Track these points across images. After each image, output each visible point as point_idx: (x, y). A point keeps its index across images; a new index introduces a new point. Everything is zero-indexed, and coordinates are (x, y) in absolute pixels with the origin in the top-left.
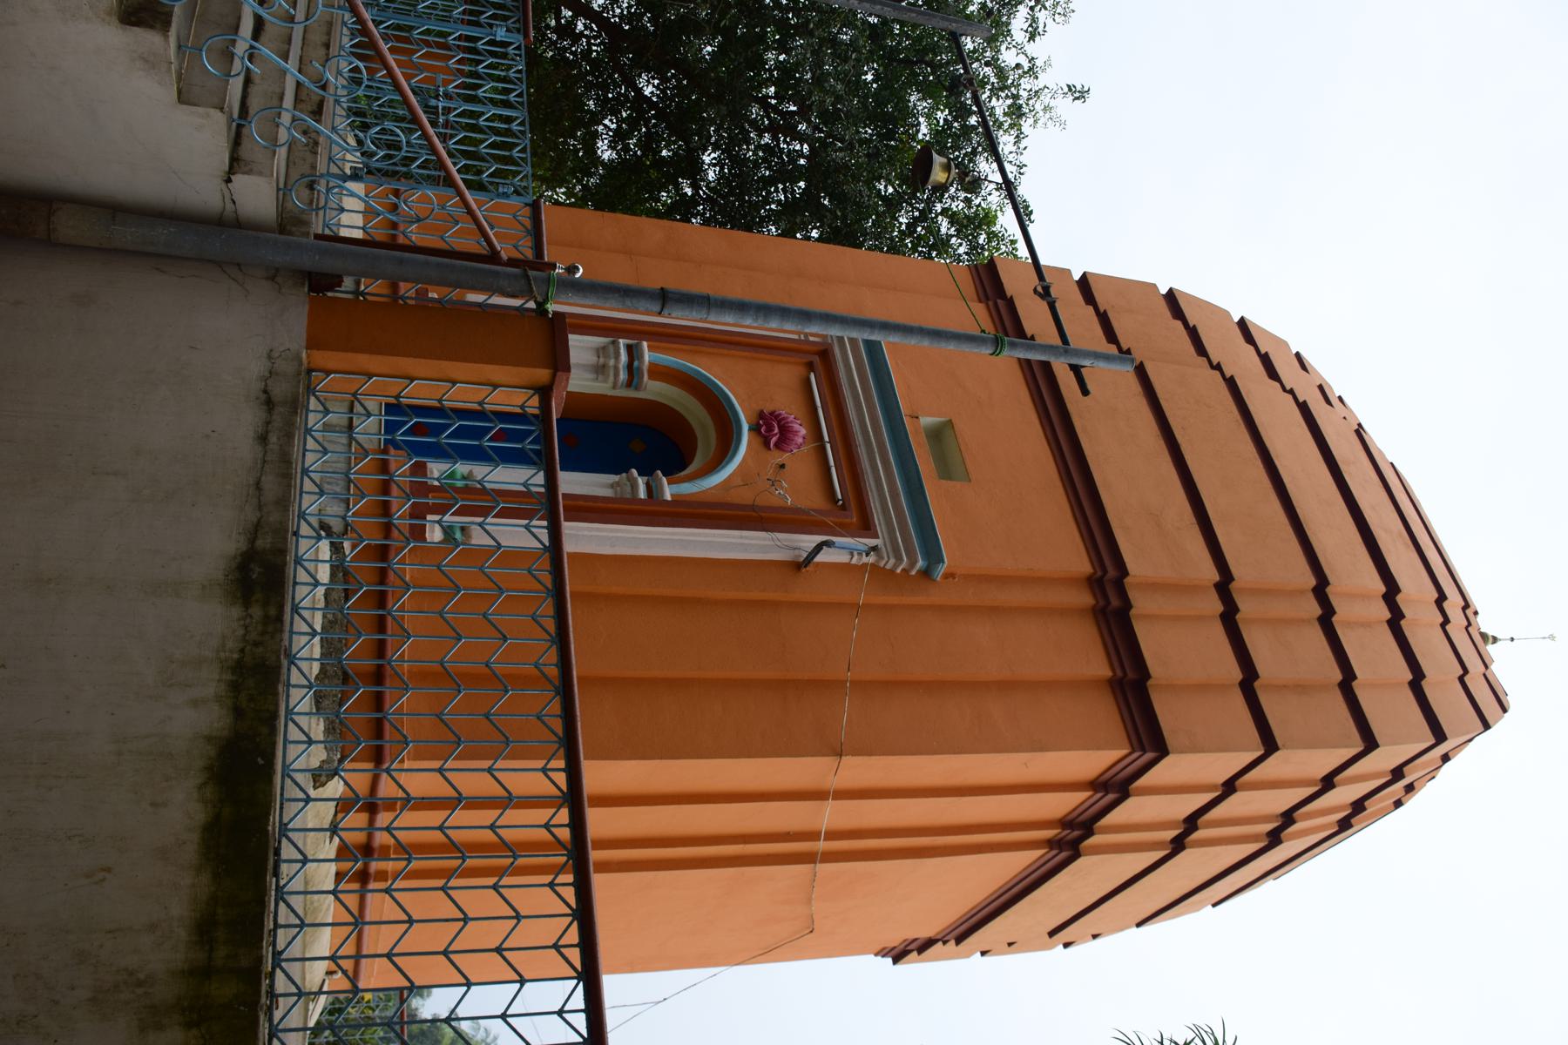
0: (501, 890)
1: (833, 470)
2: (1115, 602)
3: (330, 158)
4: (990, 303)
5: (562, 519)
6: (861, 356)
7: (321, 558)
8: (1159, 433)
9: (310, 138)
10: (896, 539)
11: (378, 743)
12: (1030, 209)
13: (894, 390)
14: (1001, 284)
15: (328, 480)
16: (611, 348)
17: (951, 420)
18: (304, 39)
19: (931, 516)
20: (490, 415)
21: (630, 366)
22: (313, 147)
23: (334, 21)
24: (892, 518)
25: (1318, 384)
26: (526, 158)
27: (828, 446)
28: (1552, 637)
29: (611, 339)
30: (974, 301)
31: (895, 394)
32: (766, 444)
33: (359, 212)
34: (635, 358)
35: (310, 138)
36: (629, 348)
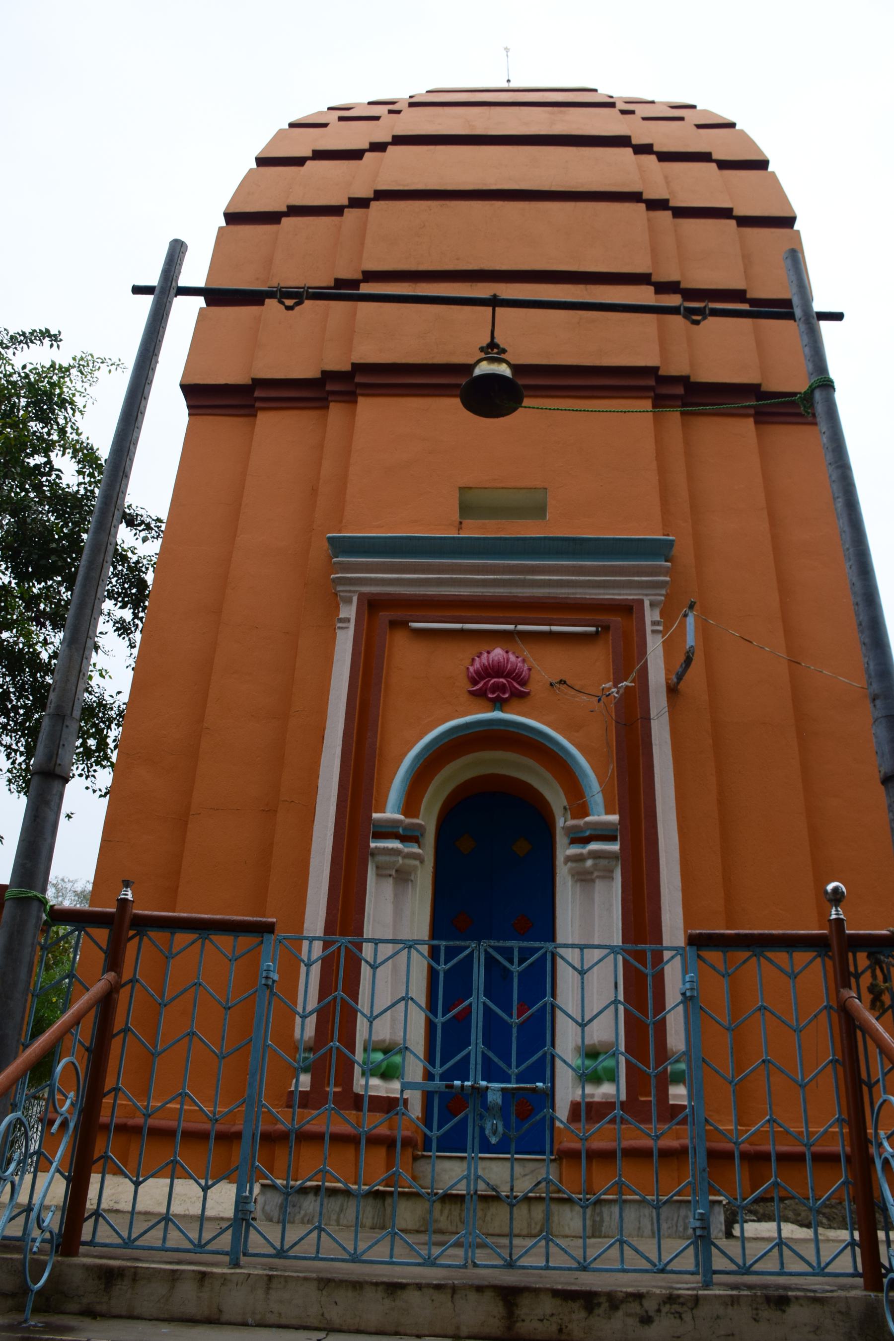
1: (555, 628)
4: (258, 404)
5: (451, 943)
6: (378, 564)
7: (130, 1209)
8: (469, 284)
9: (659, 1311)
10: (639, 582)
11: (179, 1134)
12: (44, 331)
13: (435, 538)
16: (382, 859)
17: (460, 488)
18: (377, 1333)
19: (614, 539)
22: (683, 1304)
23: (314, 1275)
25: (387, 112)
26: (521, 949)
27: (521, 627)
28: (507, 50)
31: (441, 538)
32: (522, 696)
33: (511, 1213)
34: (395, 830)
35: (659, 1311)
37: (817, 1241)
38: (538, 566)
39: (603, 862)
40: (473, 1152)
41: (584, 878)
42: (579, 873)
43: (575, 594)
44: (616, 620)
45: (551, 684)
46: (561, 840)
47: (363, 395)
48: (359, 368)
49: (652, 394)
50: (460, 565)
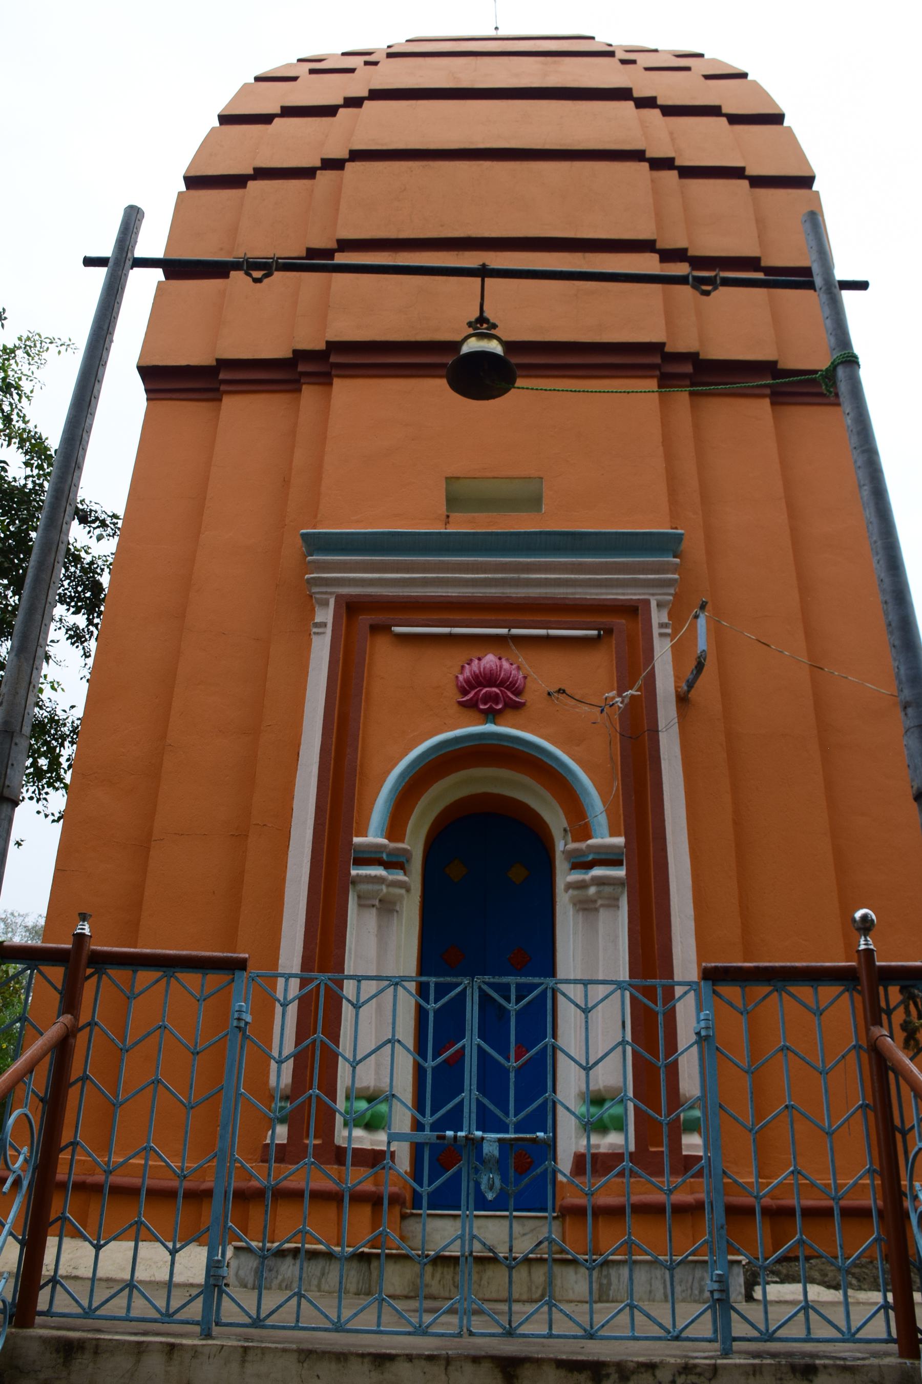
0: (591, 1062)
2: (688, 369)
3: (677, 1338)
4: (223, 388)
6: (357, 562)
8: (456, 253)
13: (419, 534)
14: (188, 368)
15: (696, 1292)
16: (363, 887)
17: (447, 478)
19: (616, 533)
20: (300, 1048)
21: (387, 865)
22: (700, 1375)
23: (294, 1346)
24: (618, 579)
26: (519, 986)
27: (515, 631)
29: (351, 886)
30: (220, 406)
31: (426, 534)
34: (378, 856)
36: (361, 862)
37: (846, 1303)
38: (533, 564)
39: (608, 889)
40: (468, 1210)
41: (586, 907)
42: (581, 902)
43: (575, 594)
44: (619, 622)
45: (549, 694)
46: (561, 865)
47: (339, 376)
48: (334, 347)
49: (658, 373)
50: (448, 563)
